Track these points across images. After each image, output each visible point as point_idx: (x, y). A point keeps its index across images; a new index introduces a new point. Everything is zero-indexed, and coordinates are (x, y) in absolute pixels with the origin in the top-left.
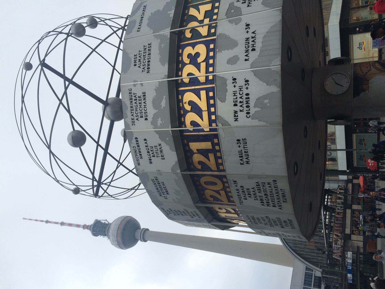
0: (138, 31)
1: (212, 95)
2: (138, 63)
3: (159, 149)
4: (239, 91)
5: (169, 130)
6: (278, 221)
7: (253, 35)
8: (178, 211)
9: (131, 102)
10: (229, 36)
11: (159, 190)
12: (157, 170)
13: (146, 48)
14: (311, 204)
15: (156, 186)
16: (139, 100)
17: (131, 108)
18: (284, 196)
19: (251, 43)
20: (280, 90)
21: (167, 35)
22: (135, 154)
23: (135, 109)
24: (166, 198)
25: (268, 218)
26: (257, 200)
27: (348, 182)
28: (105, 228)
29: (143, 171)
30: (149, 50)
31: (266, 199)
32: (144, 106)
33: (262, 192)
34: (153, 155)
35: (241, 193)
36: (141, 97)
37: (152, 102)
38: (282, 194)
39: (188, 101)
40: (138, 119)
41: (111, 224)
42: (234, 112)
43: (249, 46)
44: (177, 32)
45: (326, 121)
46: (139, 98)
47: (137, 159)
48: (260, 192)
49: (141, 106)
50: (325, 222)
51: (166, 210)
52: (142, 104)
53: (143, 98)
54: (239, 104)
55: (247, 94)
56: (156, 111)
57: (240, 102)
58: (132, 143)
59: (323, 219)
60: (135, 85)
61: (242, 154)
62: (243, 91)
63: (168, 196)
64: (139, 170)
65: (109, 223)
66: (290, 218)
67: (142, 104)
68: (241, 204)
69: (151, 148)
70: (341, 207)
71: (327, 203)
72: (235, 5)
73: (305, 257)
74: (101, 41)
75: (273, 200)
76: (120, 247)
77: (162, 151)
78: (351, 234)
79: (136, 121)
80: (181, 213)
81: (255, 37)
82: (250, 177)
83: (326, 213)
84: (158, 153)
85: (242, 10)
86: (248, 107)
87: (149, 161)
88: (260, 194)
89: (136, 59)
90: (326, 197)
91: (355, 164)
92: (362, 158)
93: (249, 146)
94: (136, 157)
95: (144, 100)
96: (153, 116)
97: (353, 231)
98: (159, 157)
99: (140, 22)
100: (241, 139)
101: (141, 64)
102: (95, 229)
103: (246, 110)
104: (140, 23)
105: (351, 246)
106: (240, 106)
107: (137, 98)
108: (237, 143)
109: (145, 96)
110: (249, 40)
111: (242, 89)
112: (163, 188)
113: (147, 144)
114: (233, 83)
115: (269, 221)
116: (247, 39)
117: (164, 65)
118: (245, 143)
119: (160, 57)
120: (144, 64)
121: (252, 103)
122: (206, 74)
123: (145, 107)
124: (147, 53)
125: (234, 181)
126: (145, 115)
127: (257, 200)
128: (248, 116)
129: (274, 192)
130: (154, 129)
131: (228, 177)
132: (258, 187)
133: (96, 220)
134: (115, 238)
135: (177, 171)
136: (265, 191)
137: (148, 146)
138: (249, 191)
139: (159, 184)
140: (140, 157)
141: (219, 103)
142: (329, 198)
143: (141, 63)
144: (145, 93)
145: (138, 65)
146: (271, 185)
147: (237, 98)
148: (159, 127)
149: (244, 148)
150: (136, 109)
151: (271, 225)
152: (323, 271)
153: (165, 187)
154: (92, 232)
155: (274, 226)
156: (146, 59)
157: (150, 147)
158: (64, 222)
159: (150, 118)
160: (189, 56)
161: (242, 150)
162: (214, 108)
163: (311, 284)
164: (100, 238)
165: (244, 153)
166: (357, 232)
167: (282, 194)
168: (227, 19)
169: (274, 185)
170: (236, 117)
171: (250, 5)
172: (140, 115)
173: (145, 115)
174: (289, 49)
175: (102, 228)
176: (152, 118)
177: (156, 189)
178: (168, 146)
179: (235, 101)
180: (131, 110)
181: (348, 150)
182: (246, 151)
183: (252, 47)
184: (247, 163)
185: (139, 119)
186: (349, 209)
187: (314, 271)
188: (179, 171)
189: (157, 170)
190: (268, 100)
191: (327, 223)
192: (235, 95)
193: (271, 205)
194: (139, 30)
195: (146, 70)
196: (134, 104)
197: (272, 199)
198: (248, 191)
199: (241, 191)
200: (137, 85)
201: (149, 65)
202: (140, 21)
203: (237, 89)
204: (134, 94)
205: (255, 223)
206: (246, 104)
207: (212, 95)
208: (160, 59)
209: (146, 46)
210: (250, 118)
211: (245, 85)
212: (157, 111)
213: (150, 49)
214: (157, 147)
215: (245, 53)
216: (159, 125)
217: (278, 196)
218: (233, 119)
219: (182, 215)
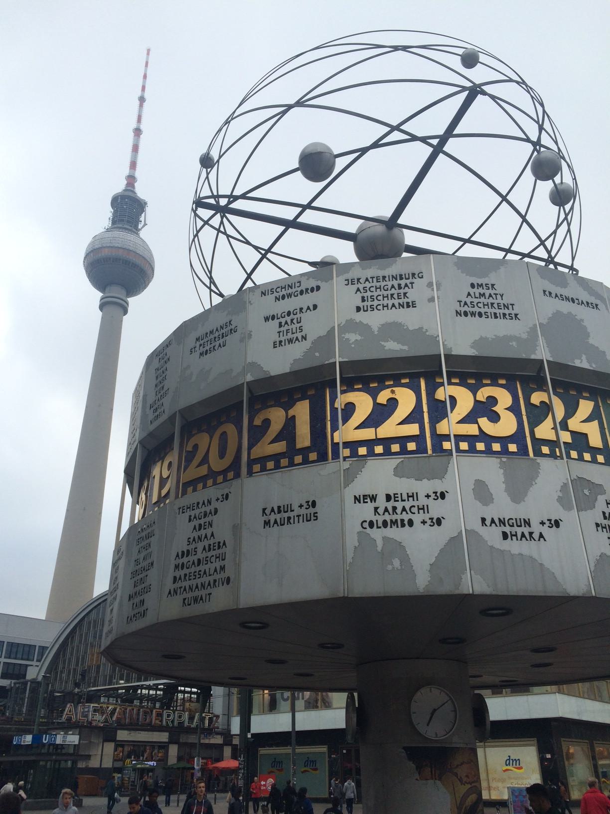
0: (544, 291)
1: (409, 449)
3: (295, 336)
4: (418, 506)
5: (335, 357)
10: (534, 483)
11: (208, 335)
13: (508, 309)
15: (217, 330)
16: (398, 294)
17: (381, 278)
18: (196, 600)
19: (519, 530)
20: (421, 591)
21: (535, 354)
22: (285, 286)
25: (150, 567)
26: (189, 543)
27: (227, 735)
28: (128, 222)
29: (250, 302)
30: (504, 315)
31: (189, 561)
32: (385, 305)
33: (205, 555)
34: (283, 324)
35: (203, 509)
36: (405, 297)
38: (200, 597)
39: (397, 398)
40: (358, 292)
41: (137, 234)
42: (373, 495)
43: (513, 526)
44: (542, 375)
45: (355, 690)
46: (402, 295)
47: (274, 290)
48: (204, 549)
49: (386, 299)
51: (168, 350)
52: (391, 299)
53: (403, 303)
54: (389, 506)
55: (411, 523)
56: (375, 329)
57: (394, 508)
58: (307, 279)
60: (430, 285)
61: (285, 512)
62: (419, 513)
64: (251, 293)
66: (149, 613)
67: (391, 299)
68: (179, 509)
69: (297, 318)
70: (173, 722)
71: (181, 692)
72: (599, 497)
73: (68, 644)
74: (523, 213)
75: (187, 578)
76: (88, 254)
77: (292, 343)
78: (117, 743)
79: (355, 287)
80: (160, 382)
81: (532, 539)
82: (236, 529)
83: (160, 690)
84: (287, 335)
86: (385, 524)
87: (270, 316)
88: (200, 550)
89: (485, 287)
90: (194, 690)
91: (263, 751)
92: (277, 764)
93: (302, 527)
94: (279, 287)
95: (399, 304)
96: (365, 322)
97: (123, 746)
98: (279, 337)
99: (564, 297)
100: (317, 509)
101: (475, 298)
102: (127, 200)
103: (377, 521)
104: (561, 295)
105: (91, 742)
106: (386, 507)
108: (308, 502)
109: (408, 306)
111: (421, 511)
112: (212, 345)
113: (306, 312)
114: (435, 493)
116: (527, 523)
117: (472, 347)
120: (475, 304)
121: (393, 533)
122: (455, 436)
123: (384, 307)
124: (497, 311)
125: (227, 495)
126: (367, 306)
128: (366, 525)
129: (206, 579)
132: (215, 546)
133: (146, 203)
134: (107, 243)
135: (249, 375)
136: (207, 560)
138: (207, 527)
139: (221, 336)
140: (279, 296)
141: (391, 463)
142: (193, 696)
143: (477, 298)
144: (413, 307)
145: (472, 291)
147: (403, 500)
148: (343, 335)
149: (297, 516)
150: (380, 288)
151: (135, 573)
152: (39, 683)
153: (216, 348)
154: (120, 194)
156: (486, 309)
157: (301, 318)
159: (361, 317)
160: (493, 400)
161: (293, 511)
163: (10, 658)
164: (108, 212)
165: (286, 515)
166: (121, 754)
168: (571, 480)
170: (364, 499)
171: (600, 528)
172: (367, 296)
178: (302, 355)
179: (398, 497)
180: (377, 277)
181: (294, 736)
182: (292, 521)
183: (511, 532)
184: (267, 523)
185: (359, 295)
186: (170, 737)
187: (38, 664)
188: (249, 378)
190: (399, 568)
191: (139, 691)
192: (408, 497)
193: (177, 574)
194: (547, 293)
195: (463, 309)
196: (390, 284)
197: (191, 576)
198: (207, 524)
199: (208, 509)
200: (430, 289)
201: (473, 314)
202: (565, 296)
203: (422, 501)
204: (412, 283)
206: (391, 521)
207: (409, 449)
208: (486, 338)
210: (362, 529)
211: (432, 519)
213: (507, 316)
214: (300, 332)
216: (347, 336)
217: (197, 587)
218: (360, 492)
219: (156, 386)
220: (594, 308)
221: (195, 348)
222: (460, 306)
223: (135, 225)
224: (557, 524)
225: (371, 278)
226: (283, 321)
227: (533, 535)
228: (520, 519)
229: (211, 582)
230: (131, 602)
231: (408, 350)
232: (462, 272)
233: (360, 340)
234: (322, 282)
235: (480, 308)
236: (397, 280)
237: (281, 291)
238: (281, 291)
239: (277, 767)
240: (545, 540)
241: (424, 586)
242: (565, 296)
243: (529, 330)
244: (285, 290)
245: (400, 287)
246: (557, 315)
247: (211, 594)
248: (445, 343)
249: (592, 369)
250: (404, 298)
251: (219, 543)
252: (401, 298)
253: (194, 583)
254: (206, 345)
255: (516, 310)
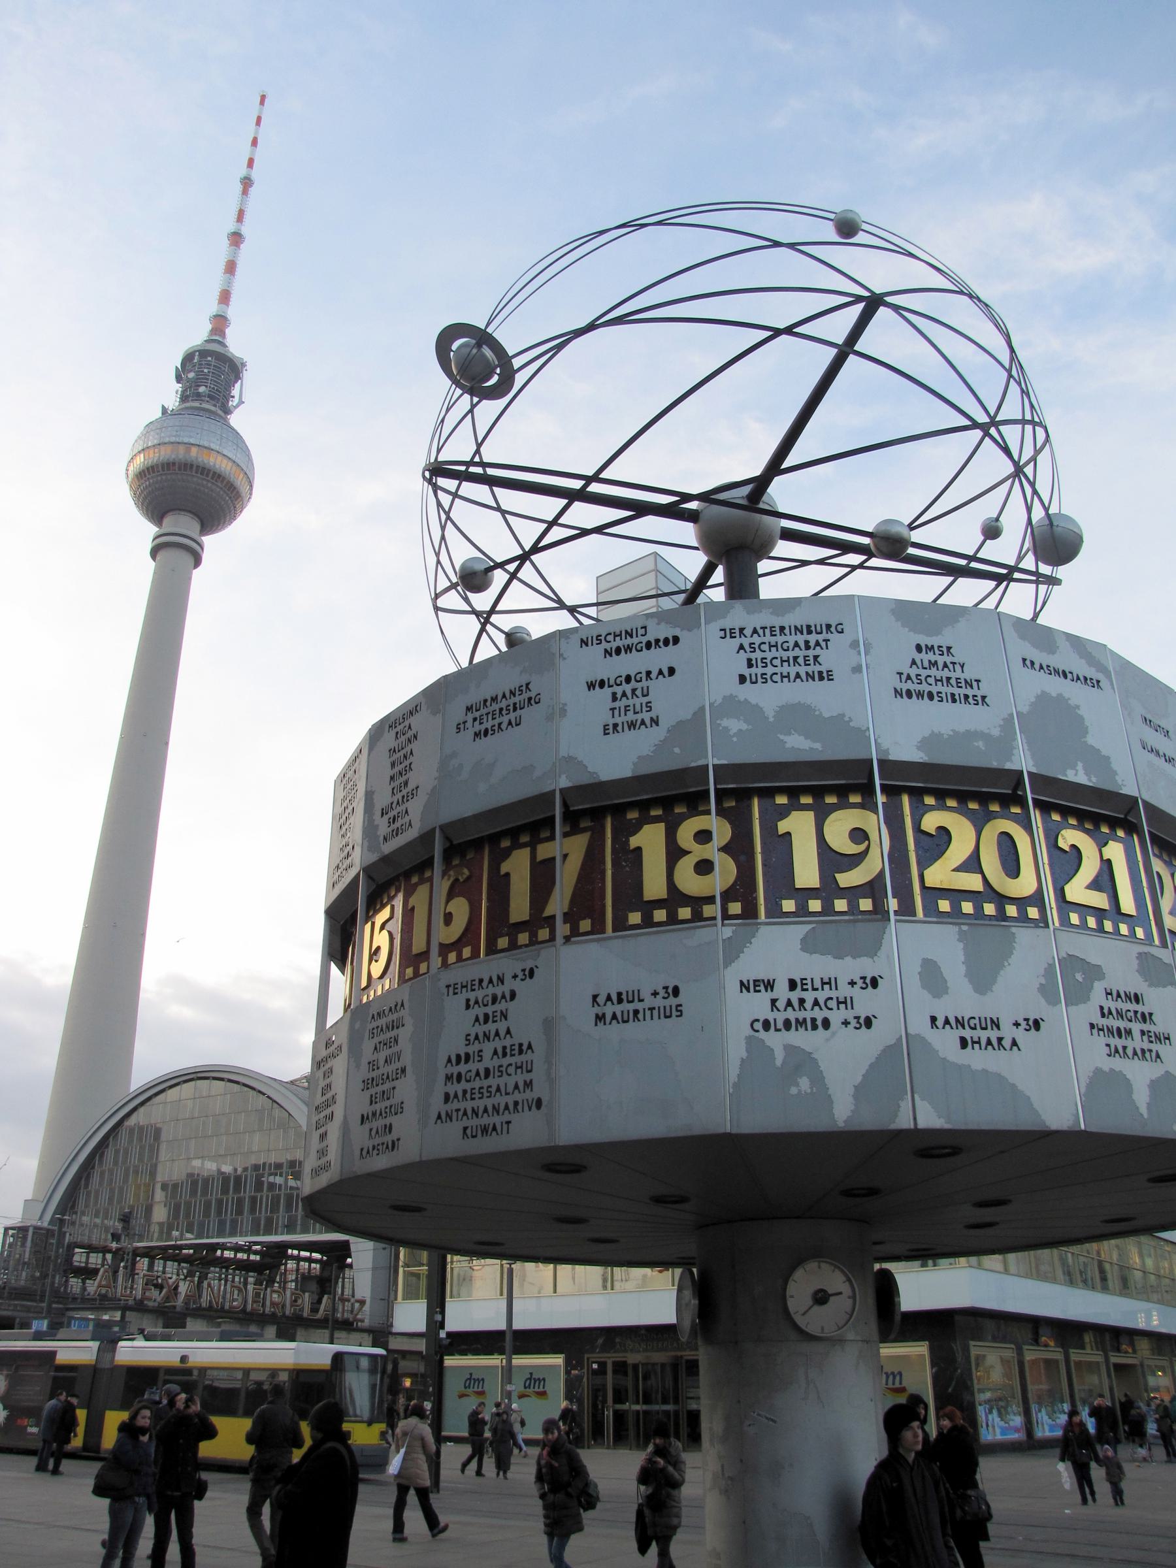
0: (1024, 660)
2: (927, 657)
3: (639, 717)
4: (837, 998)
5: (706, 757)
6: (391, 1106)
7: (1007, 1043)
8: (410, 764)
9: (798, 630)
10: (1006, 964)
11: (488, 704)
12: (565, 704)
13: (972, 688)
14: (418, 1210)
15: (504, 696)
16: (805, 657)
17: (778, 629)
18: (485, 1130)
19: (984, 1035)
20: (840, 1125)
23: (777, 643)
24: (460, 728)
25: (399, 1076)
26: (467, 1042)
29: (561, 655)
30: (966, 697)
31: (470, 1071)
33: (496, 1062)
34: (619, 696)
35: (491, 990)
36: (817, 663)
37: (802, 702)
38: (491, 1126)
40: (742, 651)
42: (769, 981)
43: (975, 1029)
44: (1020, 793)
45: (693, 1264)
47: (602, 638)
48: (495, 1053)
50: (224, 1247)
51: (414, 721)
52: (794, 665)
53: (813, 672)
54: (795, 996)
55: (826, 1024)
56: (770, 714)
57: (802, 1001)
59: (234, 1240)
61: (629, 1002)
62: (838, 1009)
63: (470, 734)
64: (562, 640)
65: (228, 411)
67: (794, 665)
69: (642, 688)
71: (292, 1257)
75: (468, 1096)
77: (634, 729)
79: (736, 642)
80: (401, 774)
81: (1001, 1048)
82: (549, 1025)
83: (256, 1253)
84: (626, 715)
85: (1082, 1006)
86: (787, 1024)
87: (596, 681)
90: (316, 1256)
91: (450, 1361)
92: (535, 1384)
94: (610, 634)
95: (807, 673)
96: (754, 702)
98: (613, 717)
100: (681, 999)
102: (209, 358)
103: (775, 1020)
104: (1048, 666)
107: (814, 649)
108: (666, 988)
109: (821, 678)
110: (992, 1029)
111: (842, 1006)
112: (496, 722)
113: (657, 678)
115: (388, 1078)
116: (996, 1024)
117: (919, 748)
118: (668, 1014)
119: (945, 736)
120: (923, 678)
121: (800, 1038)
123: (782, 677)
124: (956, 691)
126: (756, 675)
127: (467, 1042)
128: (758, 1026)
129: (500, 1100)
130: (711, 705)
131: (546, 953)
132: (514, 1050)
133: (244, 365)
135: (564, 777)
137: (651, 679)
138: (498, 1018)
139: (511, 708)
140: (611, 648)
141: (799, 931)
142: (313, 1265)
143: (926, 668)
144: (829, 680)
146: (524, 1092)
149: (649, 1009)
150: (776, 646)
151: (368, 1084)
153: (504, 726)
154: (200, 348)
155: (367, 1094)
156: (939, 688)
157: (648, 687)
158: (242, 246)
159: (748, 692)
161: (642, 1000)
162: (845, 909)
165: (631, 1007)
167: (494, 1125)
168: (1058, 959)
169: (525, 1102)
170: (755, 986)
171: (1095, 1031)
172: (756, 659)
173: (756, 675)
174: (955, 1151)
175: (207, 379)
176: (745, 699)
177: (494, 696)
179: (806, 984)
180: (771, 628)
181: (508, 1337)
182: (640, 1016)
183: (972, 1037)
184: (600, 1018)
188: (564, 782)
189: (565, 704)
191: (219, 1253)
192: (823, 983)
194: (1028, 663)
195: (905, 687)
196: (791, 640)
197: (475, 1093)
198: (498, 1014)
199: (498, 991)
200: (853, 652)
201: (920, 695)
202: (1054, 668)
203: (844, 991)
204: (827, 641)
205: (373, 1029)
206: (797, 1020)
208: (940, 735)
209: (979, 689)
211: (857, 1018)
212: (771, 719)
213: (970, 700)
214: (647, 711)
215: (956, 1018)
216: (725, 723)
217: (486, 1110)
218: (749, 975)
219: (392, 778)
220: (1094, 687)
221: (465, 723)
222: (901, 681)
223: (223, 403)
224: (1037, 1025)
225: (761, 628)
226: (619, 690)
227: (1003, 1042)
228: (986, 1018)
229: (509, 1104)
230: (367, 1126)
231: (822, 751)
232: (903, 626)
233: (747, 729)
234: (682, 630)
235: (931, 685)
236: (802, 634)
237: (615, 640)
238: (615, 640)
239: (534, 1388)
240: (1019, 1050)
241: (845, 1118)
242: (1054, 668)
243: (1002, 723)
244: (621, 639)
245: (808, 647)
246: (1043, 698)
247: (510, 1122)
248: (879, 741)
249: (1091, 784)
250: (815, 664)
251: (521, 1045)
252: (809, 665)
253: (480, 1104)
254: (485, 720)
255: (984, 689)
